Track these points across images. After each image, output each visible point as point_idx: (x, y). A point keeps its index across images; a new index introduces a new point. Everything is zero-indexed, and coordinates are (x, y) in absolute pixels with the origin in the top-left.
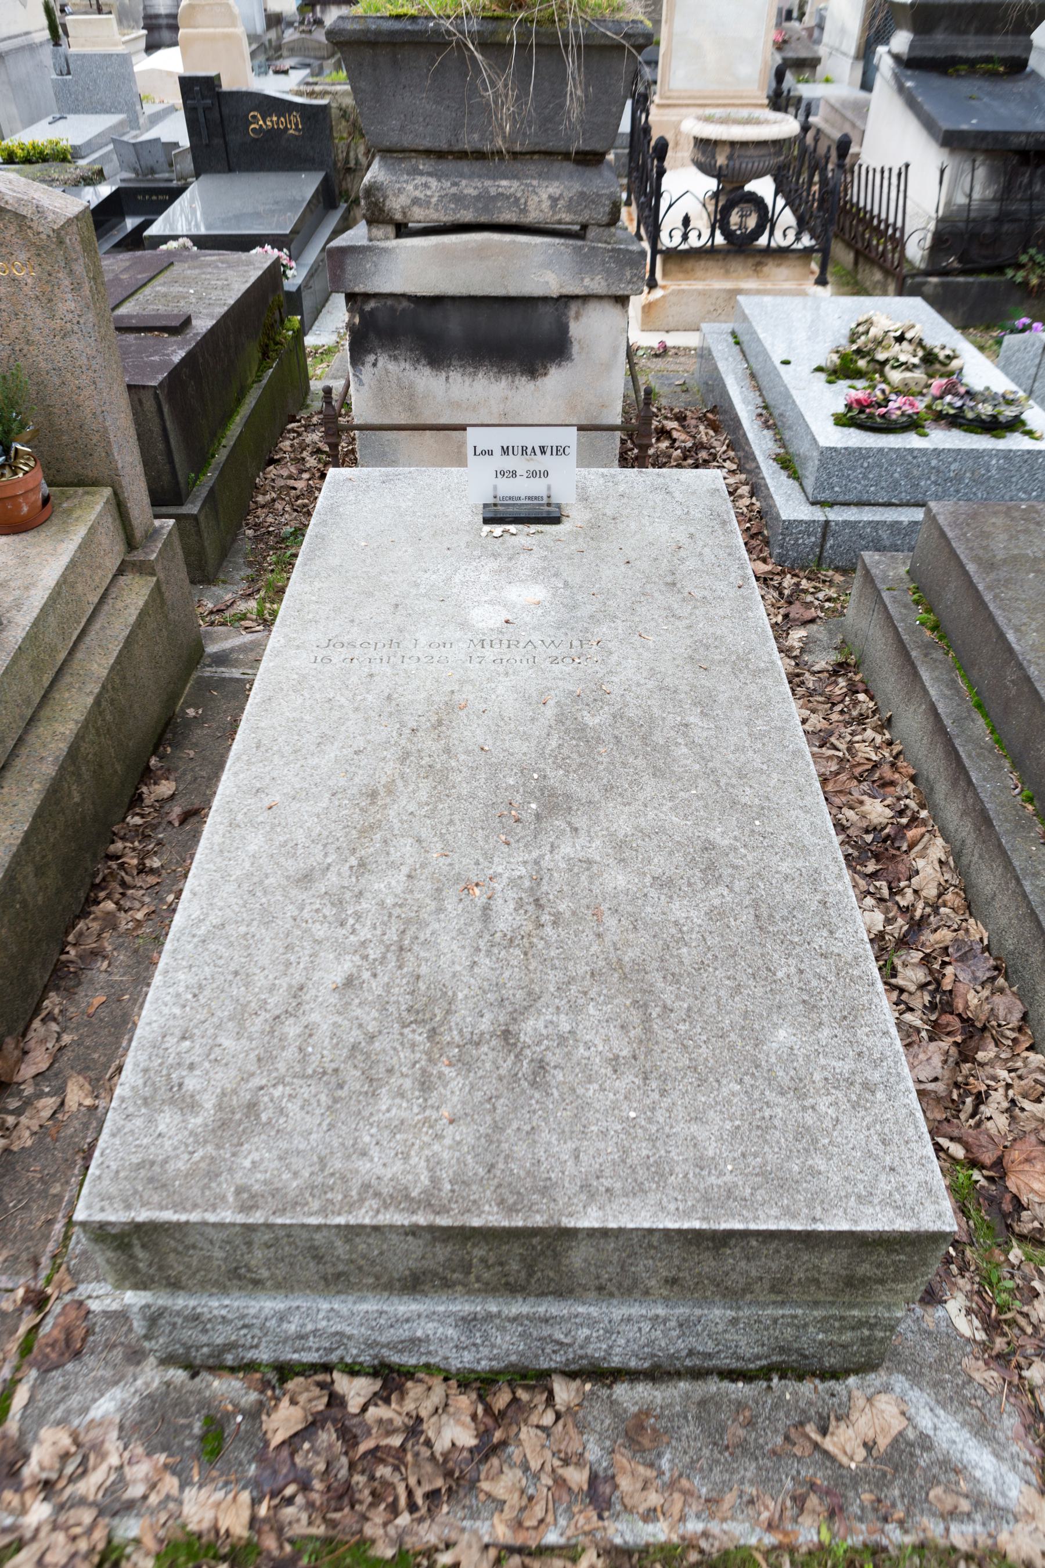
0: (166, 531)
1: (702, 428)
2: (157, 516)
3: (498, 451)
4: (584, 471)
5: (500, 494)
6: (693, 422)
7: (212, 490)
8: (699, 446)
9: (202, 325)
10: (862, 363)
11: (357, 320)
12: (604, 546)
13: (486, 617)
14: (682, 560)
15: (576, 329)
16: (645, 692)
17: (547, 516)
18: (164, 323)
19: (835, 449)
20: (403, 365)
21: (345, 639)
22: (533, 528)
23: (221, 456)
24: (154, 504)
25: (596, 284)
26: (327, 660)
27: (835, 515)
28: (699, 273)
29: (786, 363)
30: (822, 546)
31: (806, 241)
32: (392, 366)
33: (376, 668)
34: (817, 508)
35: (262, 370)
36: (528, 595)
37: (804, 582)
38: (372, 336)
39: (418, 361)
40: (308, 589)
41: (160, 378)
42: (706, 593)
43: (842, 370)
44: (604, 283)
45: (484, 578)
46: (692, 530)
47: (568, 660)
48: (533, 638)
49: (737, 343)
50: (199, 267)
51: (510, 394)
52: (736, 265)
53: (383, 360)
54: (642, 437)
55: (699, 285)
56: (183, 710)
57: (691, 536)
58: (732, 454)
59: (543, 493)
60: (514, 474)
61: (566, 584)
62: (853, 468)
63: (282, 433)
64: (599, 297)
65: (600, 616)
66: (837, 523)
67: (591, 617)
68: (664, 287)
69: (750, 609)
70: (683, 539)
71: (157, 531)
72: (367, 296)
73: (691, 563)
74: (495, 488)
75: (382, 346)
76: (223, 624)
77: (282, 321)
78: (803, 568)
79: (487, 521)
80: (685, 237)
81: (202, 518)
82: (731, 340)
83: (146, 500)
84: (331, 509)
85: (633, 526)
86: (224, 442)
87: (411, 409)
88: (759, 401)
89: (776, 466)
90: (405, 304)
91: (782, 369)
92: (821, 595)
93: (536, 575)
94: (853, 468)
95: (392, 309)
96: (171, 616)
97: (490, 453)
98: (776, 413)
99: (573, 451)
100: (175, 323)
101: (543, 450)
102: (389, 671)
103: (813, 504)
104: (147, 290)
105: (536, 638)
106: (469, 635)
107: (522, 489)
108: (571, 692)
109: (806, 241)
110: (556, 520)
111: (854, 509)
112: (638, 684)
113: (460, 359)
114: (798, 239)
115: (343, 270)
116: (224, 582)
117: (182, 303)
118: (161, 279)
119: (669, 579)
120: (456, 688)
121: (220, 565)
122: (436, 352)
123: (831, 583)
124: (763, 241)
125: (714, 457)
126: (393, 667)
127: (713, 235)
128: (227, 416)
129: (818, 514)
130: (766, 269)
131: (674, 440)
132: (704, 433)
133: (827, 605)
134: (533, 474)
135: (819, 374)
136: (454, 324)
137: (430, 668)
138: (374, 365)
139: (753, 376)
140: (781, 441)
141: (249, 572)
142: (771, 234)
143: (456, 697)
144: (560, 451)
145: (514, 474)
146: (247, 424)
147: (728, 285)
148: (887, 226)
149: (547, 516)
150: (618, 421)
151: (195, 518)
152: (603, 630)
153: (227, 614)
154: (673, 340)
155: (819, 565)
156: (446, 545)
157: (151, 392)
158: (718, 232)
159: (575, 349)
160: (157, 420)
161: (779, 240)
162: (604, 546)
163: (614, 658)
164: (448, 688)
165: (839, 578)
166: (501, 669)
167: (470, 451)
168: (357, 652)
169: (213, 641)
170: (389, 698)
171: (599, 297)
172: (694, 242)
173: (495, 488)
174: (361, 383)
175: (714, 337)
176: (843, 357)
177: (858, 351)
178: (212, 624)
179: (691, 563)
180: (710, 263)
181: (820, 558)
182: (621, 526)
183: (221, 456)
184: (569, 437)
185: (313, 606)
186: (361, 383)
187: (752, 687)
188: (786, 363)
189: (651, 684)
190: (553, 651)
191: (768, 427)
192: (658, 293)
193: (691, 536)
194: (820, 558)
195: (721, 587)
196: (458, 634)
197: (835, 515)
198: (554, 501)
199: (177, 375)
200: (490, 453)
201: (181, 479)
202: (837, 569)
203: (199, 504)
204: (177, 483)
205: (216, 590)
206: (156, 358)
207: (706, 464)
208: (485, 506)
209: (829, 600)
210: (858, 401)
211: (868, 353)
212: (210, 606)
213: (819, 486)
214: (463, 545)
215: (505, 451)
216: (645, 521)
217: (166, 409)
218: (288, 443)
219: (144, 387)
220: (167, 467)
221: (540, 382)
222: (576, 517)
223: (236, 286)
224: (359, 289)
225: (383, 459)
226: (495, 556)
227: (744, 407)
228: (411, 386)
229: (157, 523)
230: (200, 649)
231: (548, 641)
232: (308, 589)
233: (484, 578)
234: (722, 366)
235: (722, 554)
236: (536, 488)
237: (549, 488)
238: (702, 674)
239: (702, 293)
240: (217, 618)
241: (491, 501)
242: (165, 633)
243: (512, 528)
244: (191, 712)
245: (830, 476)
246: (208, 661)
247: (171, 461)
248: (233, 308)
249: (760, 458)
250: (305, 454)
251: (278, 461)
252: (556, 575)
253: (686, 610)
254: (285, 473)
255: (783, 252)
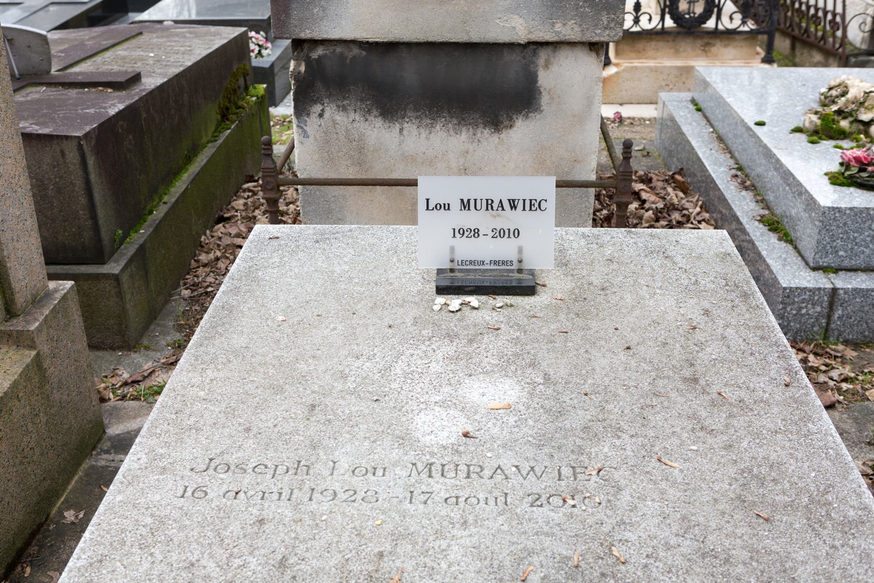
0: (58, 296)
1: (670, 190)
2: (52, 277)
3: (456, 205)
4: (561, 231)
5: (459, 257)
6: (660, 184)
7: (142, 249)
8: (671, 208)
9: (151, 82)
10: (844, 124)
11: (303, 68)
12: (594, 324)
13: (437, 428)
14: (701, 346)
15: (545, 79)
16: (679, 561)
17: (517, 285)
18: (110, 79)
19: (839, 210)
20: (352, 115)
21: (233, 459)
22: (500, 300)
23: (159, 213)
24: (48, 262)
25: (569, 30)
26: (201, 492)
27: (844, 282)
28: (651, 53)
29: (761, 124)
30: (829, 317)
31: (751, 25)
32: (340, 117)
33: (274, 509)
34: (819, 275)
35: (218, 130)
36: (497, 393)
37: (811, 357)
38: (319, 85)
39: (369, 112)
40: (196, 380)
41: (88, 129)
42: (743, 394)
43: (824, 131)
44: (577, 29)
45: (435, 367)
46: (706, 304)
47: (556, 501)
48: (503, 462)
49: (699, 110)
50: (166, 37)
51: (471, 147)
52: (686, 45)
53: (330, 111)
54: (627, 191)
55: (651, 63)
56: (60, 513)
57: (706, 313)
58: (706, 215)
59: (513, 256)
60: (476, 233)
61: (547, 377)
62: (860, 231)
63: (237, 192)
64: (572, 44)
65: (598, 427)
66: (846, 291)
67: (586, 429)
68: (617, 65)
69: (810, 419)
70: (697, 317)
71: (48, 295)
72: (315, 43)
73: (713, 350)
74: (452, 249)
75: (329, 96)
76: (136, 398)
77: (247, 88)
78: (808, 342)
79: (441, 290)
80: (636, 21)
81: (125, 279)
82: (692, 107)
83: (38, 258)
84: (249, 273)
85: (629, 299)
86: (166, 198)
87: (360, 164)
88: (731, 162)
89: (763, 229)
90: (356, 51)
91: (758, 130)
92: (835, 374)
93: (507, 365)
94: (860, 231)
95: (342, 56)
96: (56, 396)
97: (447, 207)
98: (753, 174)
99: (551, 206)
100: (122, 79)
101: (513, 205)
102: (288, 513)
103: (814, 269)
104: (108, 55)
105: (507, 461)
106: (411, 456)
107: (486, 251)
108: (566, 559)
109: (751, 25)
110: (529, 290)
111: (862, 276)
112: (668, 547)
113: (416, 110)
114: (744, 23)
115: (288, 15)
116: (147, 348)
117: (139, 64)
118: (126, 45)
119: (687, 373)
120: (387, 547)
121: (146, 327)
122: (389, 102)
123: (844, 361)
124: (711, 24)
125: (688, 218)
126: (296, 508)
127: (663, 19)
128: (175, 173)
129: (823, 281)
130: (713, 49)
131: (644, 202)
132: (674, 195)
133: (845, 386)
134: (501, 233)
135: (798, 135)
136: (410, 73)
137: (350, 510)
138: (321, 115)
139: (720, 139)
140: (763, 202)
141: (178, 336)
142: (719, 18)
143: (386, 564)
144: (534, 205)
145: (476, 233)
146: (193, 182)
147: (679, 63)
148: (826, 13)
149: (517, 285)
150: (593, 177)
151: (116, 278)
152: (605, 450)
153: (142, 386)
154: (627, 111)
155: (826, 338)
156: (387, 321)
157: (75, 143)
158: (667, 17)
159: (544, 100)
160: (80, 172)
161: (726, 23)
162: (594, 324)
163: (625, 498)
164: (373, 548)
165: (850, 354)
166: (456, 515)
167: (422, 205)
168: (248, 479)
169: (120, 419)
170: (283, 564)
171: (572, 44)
172: (645, 24)
173: (452, 249)
174: (305, 135)
175: (676, 105)
176: (823, 117)
177: (839, 112)
178: (123, 398)
179: (713, 350)
180: (661, 44)
181: (827, 330)
182: (613, 299)
183: (159, 213)
184: (544, 187)
185: (198, 406)
186: (305, 135)
187: (845, 556)
188: (761, 124)
189: (687, 546)
190: (533, 485)
191: (746, 188)
192: (611, 70)
193: (706, 313)
194: (827, 330)
195: (760, 383)
196: (395, 454)
197: (844, 282)
198: (526, 266)
199: (108, 130)
200: (447, 207)
201: (105, 235)
202: (846, 343)
203: (123, 263)
204: (99, 240)
205: (136, 357)
206: (92, 111)
207: (680, 224)
208: (440, 271)
209: (845, 380)
210: (858, 159)
211: (850, 114)
212: (126, 376)
213: (821, 249)
214: (409, 321)
215: (465, 205)
216: (644, 292)
217: (91, 161)
218: (241, 202)
219: (67, 137)
220: (89, 223)
221: (504, 135)
222: (555, 286)
223: (198, 51)
224: (306, 34)
225: (328, 216)
226: (451, 336)
227: (718, 169)
228: (361, 138)
229: (52, 285)
230: (99, 429)
231: (525, 467)
232: (196, 380)
233: (435, 367)
234: (685, 129)
235: (752, 337)
236: (505, 250)
237: (520, 250)
238: (763, 530)
239: (651, 69)
240: (131, 390)
241: (447, 265)
242: (43, 418)
243: (474, 300)
244: (70, 515)
245: (833, 238)
246: (106, 445)
247: (94, 217)
248: (189, 69)
249: (744, 220)
250: (257, 212)
251: (229, 219)
252: (532, 365)
253: (717, 421)
254: (233, 231)
255: (730, 34)
